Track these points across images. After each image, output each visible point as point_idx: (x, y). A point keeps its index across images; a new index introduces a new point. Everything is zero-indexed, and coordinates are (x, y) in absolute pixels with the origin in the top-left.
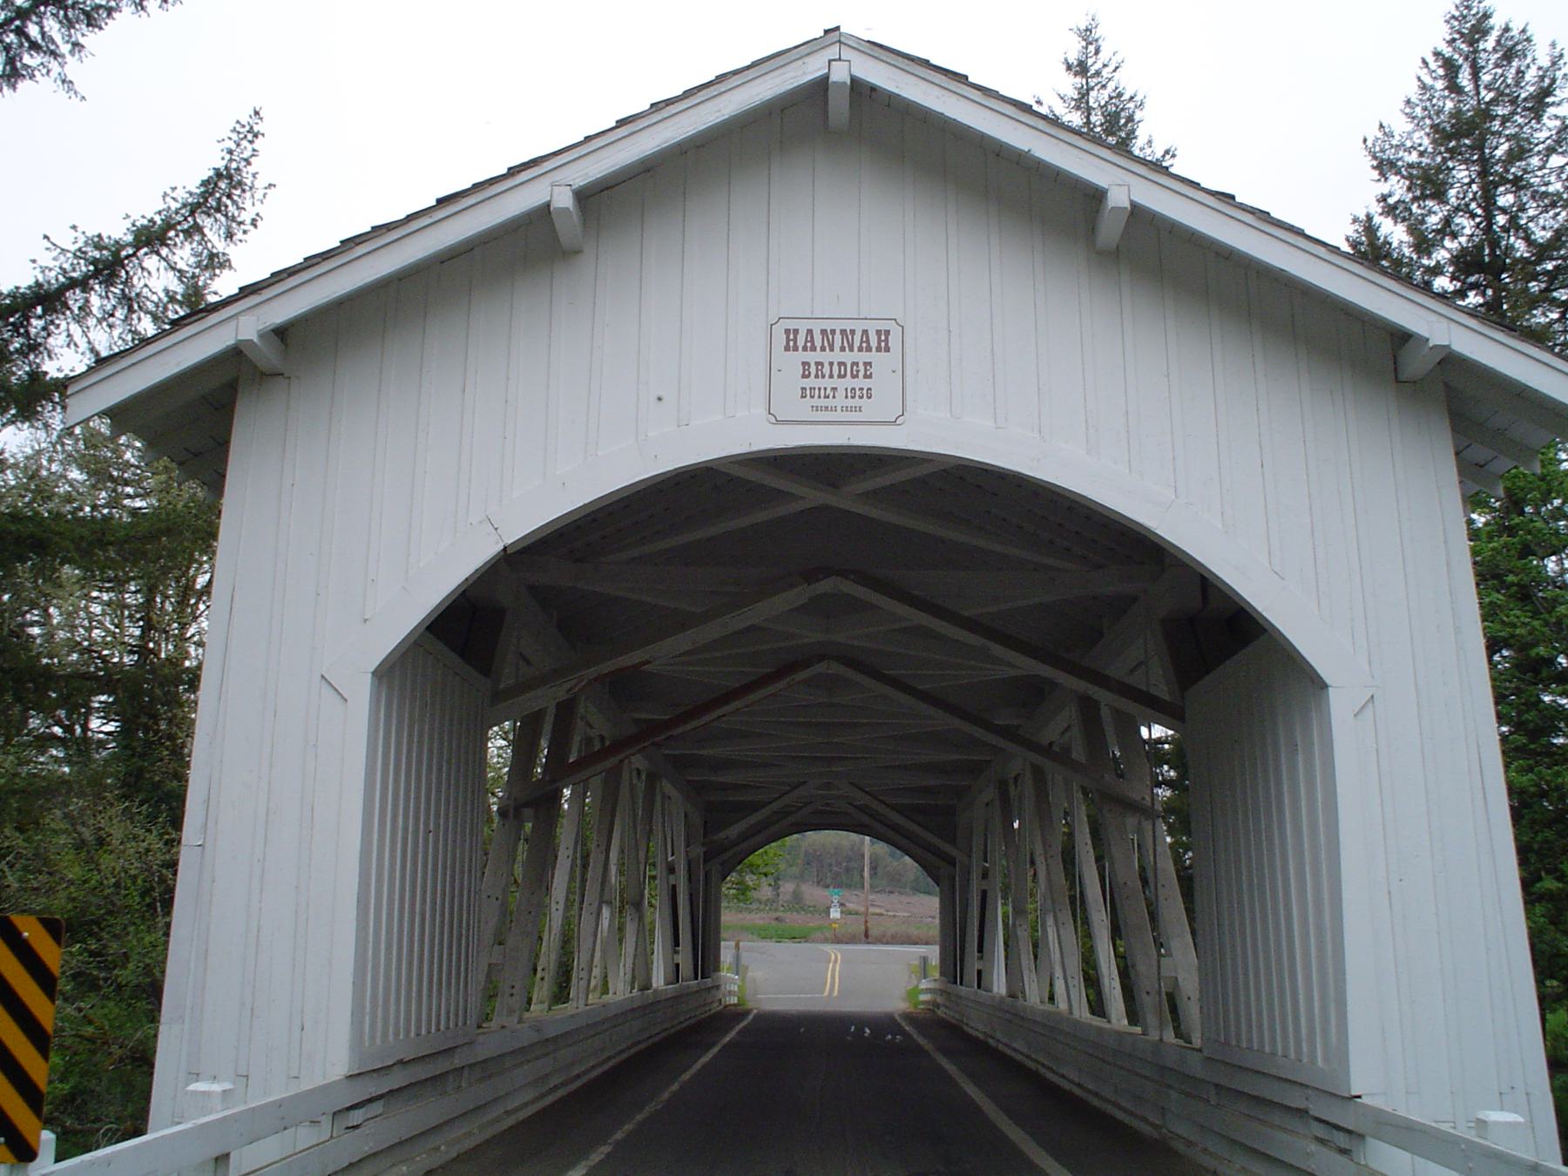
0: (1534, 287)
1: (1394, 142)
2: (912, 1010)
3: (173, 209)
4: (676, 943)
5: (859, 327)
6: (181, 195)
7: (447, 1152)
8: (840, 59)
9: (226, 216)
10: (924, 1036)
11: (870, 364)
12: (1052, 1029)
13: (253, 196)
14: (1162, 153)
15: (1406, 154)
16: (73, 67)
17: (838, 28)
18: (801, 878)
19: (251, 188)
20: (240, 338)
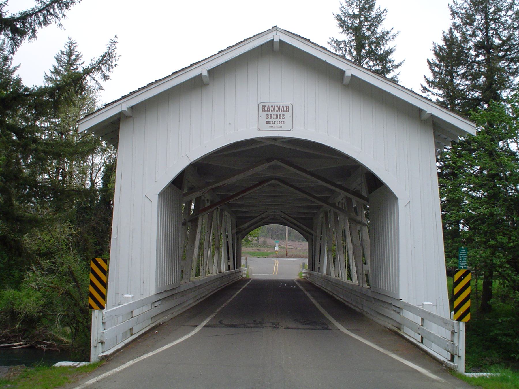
0: (501, 54)
1: (458, 6)
2: (300, 279)
3: (94, 63)
4: (229, 259)
5: (281, 105)
6: (96, 60)
7: (175, 314)
8: (277, 35)
9: (108, 64)
10: (302, 286)
11: (284, 115)
12: (337, 284)
13: (115, 59)
14: (383, 10)
15: (461, 10)
16: (62, 21)
17: (276, 26)
18: (266, 236)
19: (115, 57)
20: (123, 109)
